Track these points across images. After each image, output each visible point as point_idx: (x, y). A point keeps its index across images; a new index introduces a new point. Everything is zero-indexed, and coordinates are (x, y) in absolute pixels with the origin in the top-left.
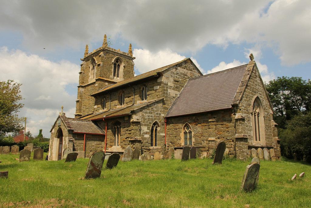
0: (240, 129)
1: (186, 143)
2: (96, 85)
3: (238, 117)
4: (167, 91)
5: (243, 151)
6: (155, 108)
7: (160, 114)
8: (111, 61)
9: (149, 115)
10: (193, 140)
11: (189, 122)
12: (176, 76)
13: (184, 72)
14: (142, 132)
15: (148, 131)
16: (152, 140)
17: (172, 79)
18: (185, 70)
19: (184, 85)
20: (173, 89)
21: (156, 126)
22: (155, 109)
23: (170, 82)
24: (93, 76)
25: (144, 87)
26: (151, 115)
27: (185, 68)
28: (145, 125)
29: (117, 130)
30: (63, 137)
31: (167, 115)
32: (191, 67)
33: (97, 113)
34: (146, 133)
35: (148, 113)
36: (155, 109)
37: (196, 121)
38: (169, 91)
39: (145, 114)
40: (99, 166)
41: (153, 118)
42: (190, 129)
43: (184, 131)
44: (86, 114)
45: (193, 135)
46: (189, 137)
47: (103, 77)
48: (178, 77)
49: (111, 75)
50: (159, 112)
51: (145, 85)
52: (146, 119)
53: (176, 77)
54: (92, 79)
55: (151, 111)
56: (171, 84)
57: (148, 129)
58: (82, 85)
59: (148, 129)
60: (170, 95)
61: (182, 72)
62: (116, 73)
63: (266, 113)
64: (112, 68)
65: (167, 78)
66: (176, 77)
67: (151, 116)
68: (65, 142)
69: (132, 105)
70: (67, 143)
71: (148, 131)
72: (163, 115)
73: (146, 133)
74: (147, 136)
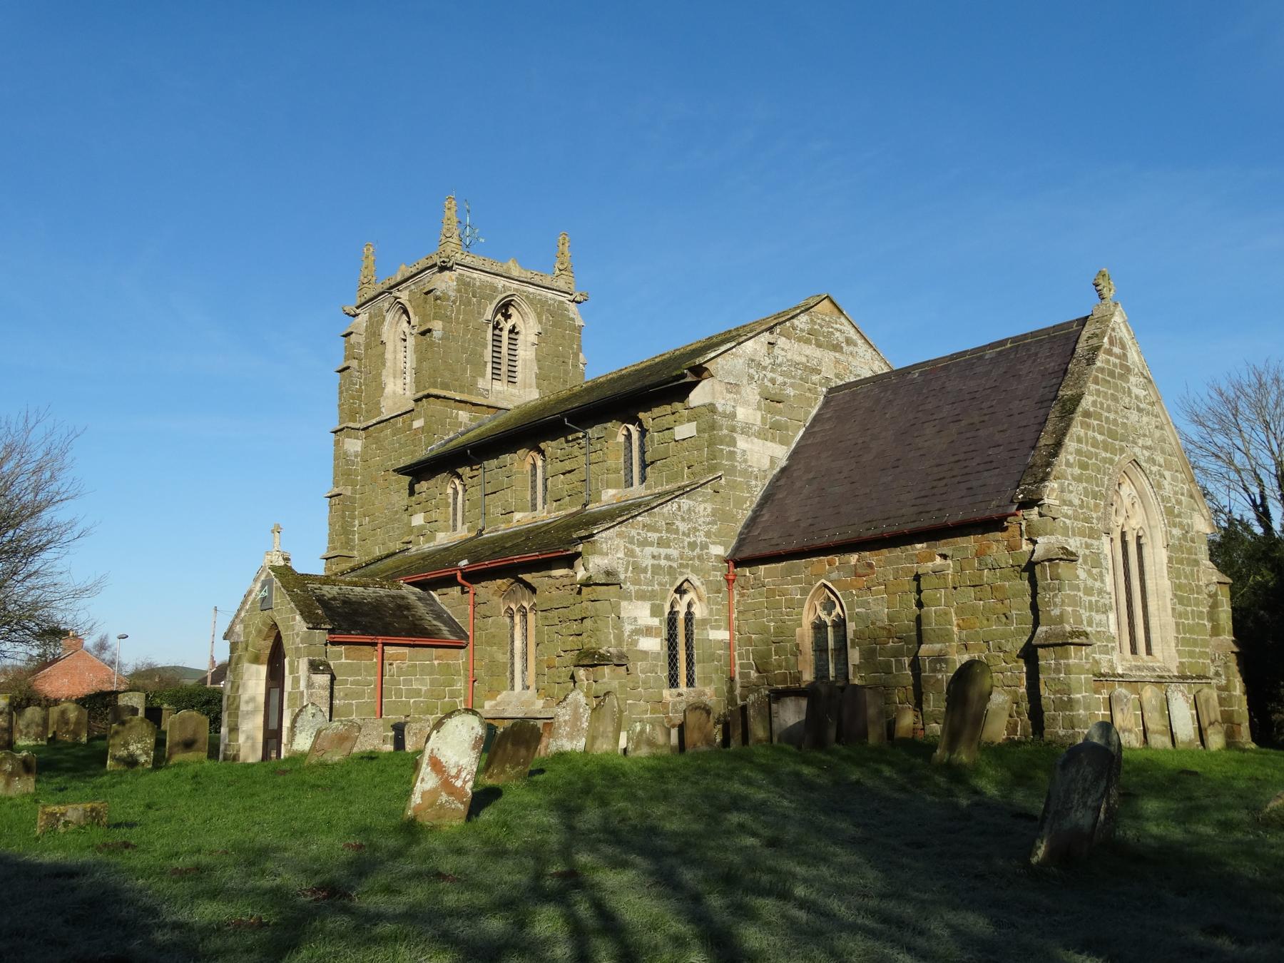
0: (1055, 605)
1: (821, 669)
2: (418, 424)
3: (1048, 551)
4: (733, 443)
5: (1070, 700)
6: (683, 519)
7: (704, 546)
8: (480, 314)
9: (655, 550)
10: (854, 656)
11: (834, 575)
12: (770, 375)
13: (804, 360)
14: (628, 628)
15: (655, 622)
16: (673, 659)
17: (752, 393)
18: (811, 350)
19: (808, 413)
20: (762, 435)
21: (687, 598)
22: (683, 526)
23: (746, 403)
24: (400, 382)
25: (630, 426)
26: (663, 551)
27: (808, 342)
28: (642, 596)
29: (517, 618)
30: (286, 660)
31: (738, 548)
32: (838, 334)
33: (427, 547)
34: (648, 632)
35: (651, 544)
36: (683, 526)
37: (860, 571)
38: (742, 443)
39: (637, 550)
40: (463, 774)
41: (675, 565)
42: (838, 608)
43: (812, 618)
44: (377, 552)
45: (850, 635)
46: (836, 642)
47: (445, 386)
48: (780, 379)
49: (483, 376)
50: (701, 538)
51: (635, 420)
52: (645, 570)
53: (773, 381)
54: (397, 389)
55: (664, 534)
56: (747, 413)
57: (653, 614)
58: (351, 425)
59: (653, 614)
60: (745, 461)
61: (797, 358)
62: (504, 368)
63: (1177, 532)
64: (485, 346)
65: (733, 387)
66: (773, 381)
67: (668, 557)
68: (296, 681)
69: (579, 508)
70: (303, 684)
71: (655, 622)
72: (718, 550)
73: (648, 632)
74: (653, 645)
